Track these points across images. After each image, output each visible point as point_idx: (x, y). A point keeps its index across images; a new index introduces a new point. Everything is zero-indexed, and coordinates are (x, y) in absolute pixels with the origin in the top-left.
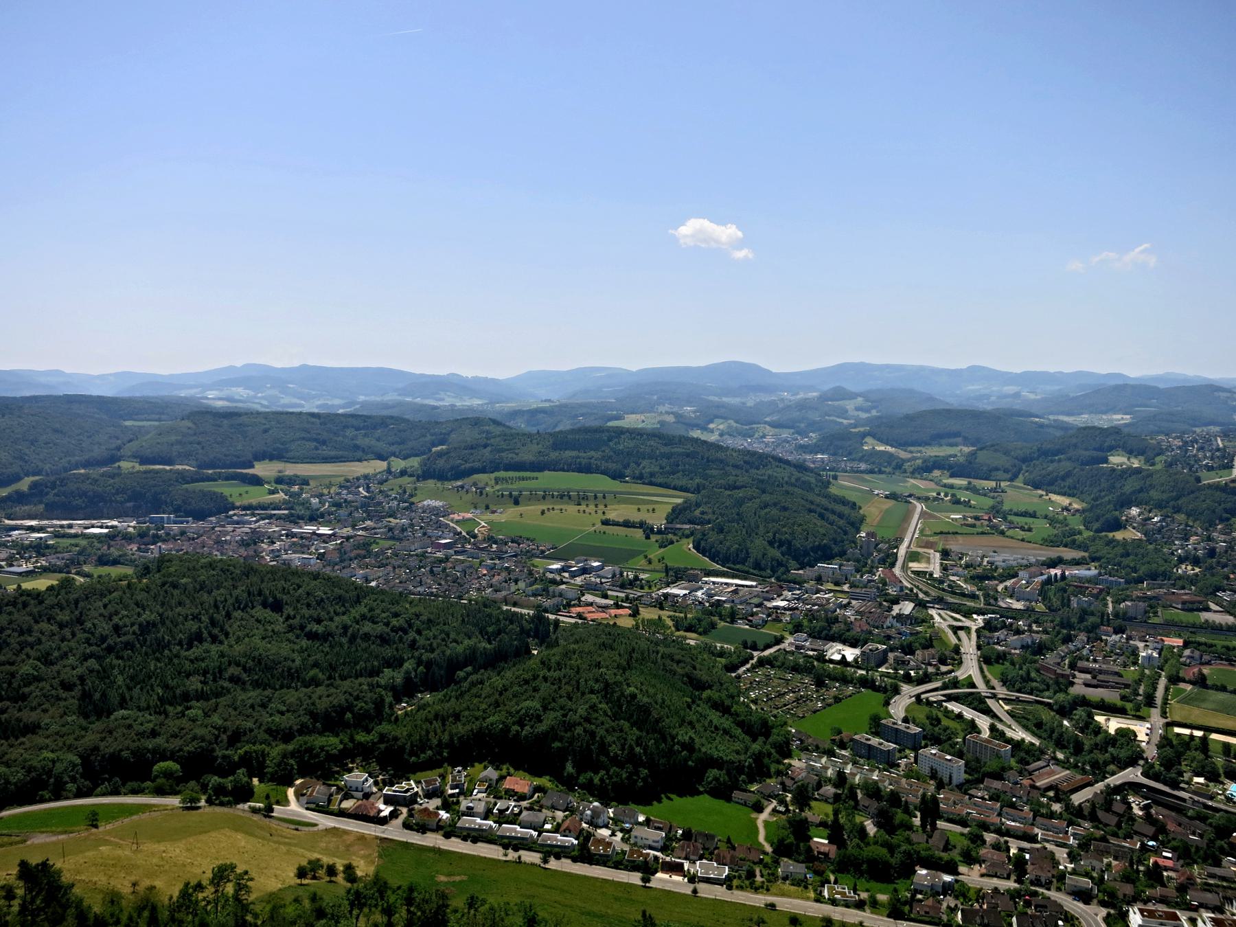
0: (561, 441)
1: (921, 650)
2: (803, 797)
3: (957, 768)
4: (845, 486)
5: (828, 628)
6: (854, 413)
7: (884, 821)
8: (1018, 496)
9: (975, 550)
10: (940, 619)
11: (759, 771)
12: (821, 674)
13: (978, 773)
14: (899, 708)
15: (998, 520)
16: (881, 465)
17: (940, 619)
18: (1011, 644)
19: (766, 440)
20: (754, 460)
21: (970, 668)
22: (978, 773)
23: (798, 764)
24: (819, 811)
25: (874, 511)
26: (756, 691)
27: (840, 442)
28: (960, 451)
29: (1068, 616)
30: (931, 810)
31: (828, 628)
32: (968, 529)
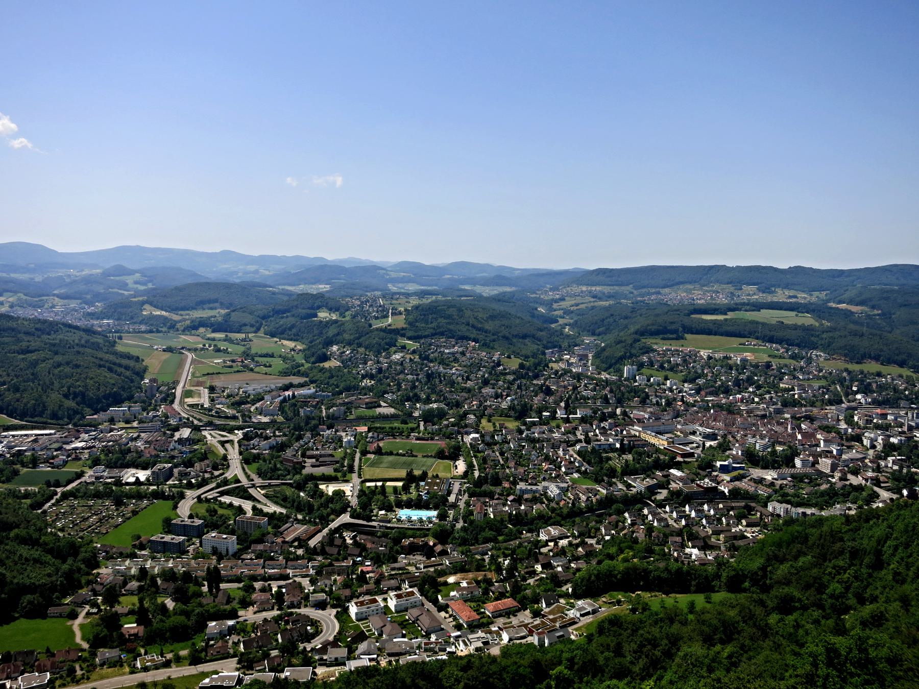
0: (499, 277)
1: (199, 461)
2: (112, 595)
3: (231, 542)
4: (129, 344)
5: (123, 458)
6: (133, 285)
7: (180, 596)
8: (261, 343)
9: (234, 384)
10: (211, 437)
11: (71, 584)
12: (118, 495)
13: (246, 542)
14: (185, 509)
15: (249, 361)
16: (156, 326)
17: (211, 437)
18: (262, 447)
19: (55, 310)
20: (45, 327)
21: (235, 469)
22: (246, 542)
23: (105, 572)
24: (128, 603)
25: (155, 364)
26: (61, 520)
27: (123, 310)
28: (218, 313)
29: (299, 422)
30: (214, 577)
31: (123, 458)
32: (228, 368)
